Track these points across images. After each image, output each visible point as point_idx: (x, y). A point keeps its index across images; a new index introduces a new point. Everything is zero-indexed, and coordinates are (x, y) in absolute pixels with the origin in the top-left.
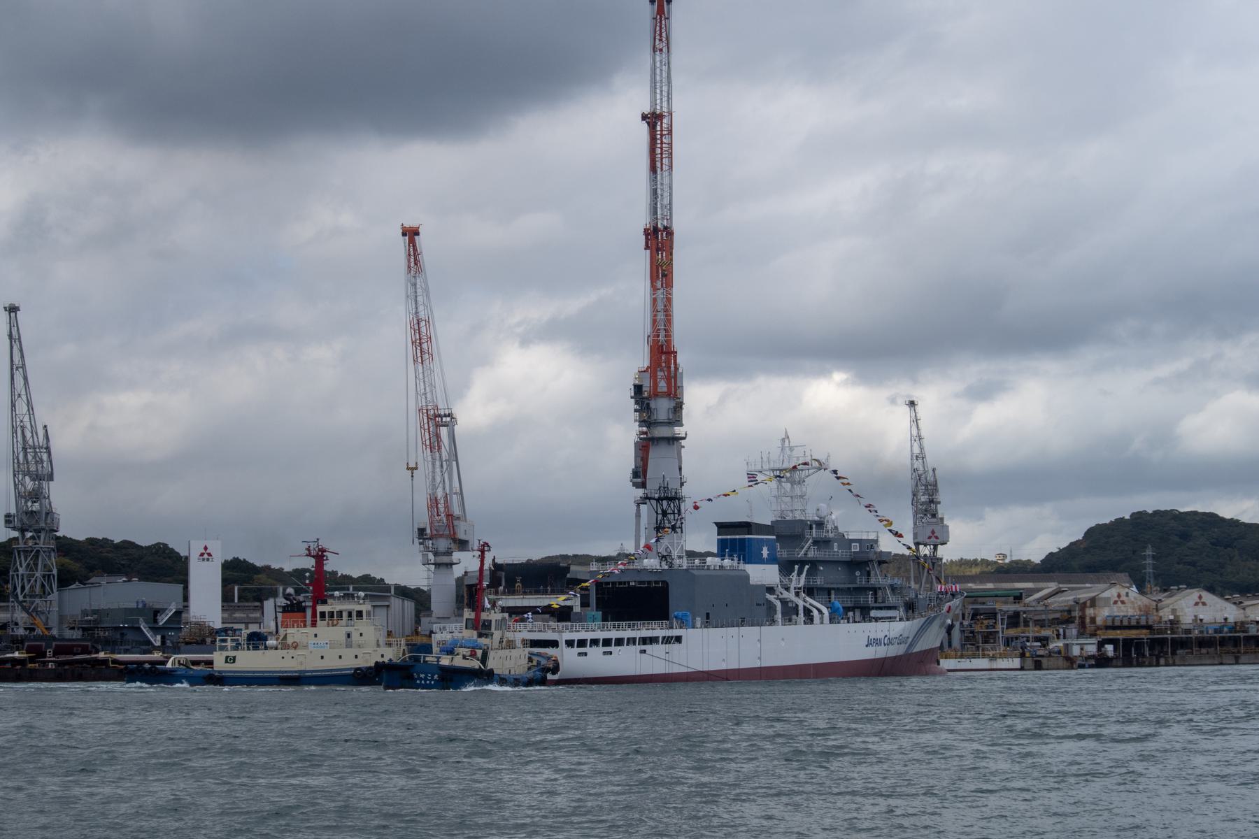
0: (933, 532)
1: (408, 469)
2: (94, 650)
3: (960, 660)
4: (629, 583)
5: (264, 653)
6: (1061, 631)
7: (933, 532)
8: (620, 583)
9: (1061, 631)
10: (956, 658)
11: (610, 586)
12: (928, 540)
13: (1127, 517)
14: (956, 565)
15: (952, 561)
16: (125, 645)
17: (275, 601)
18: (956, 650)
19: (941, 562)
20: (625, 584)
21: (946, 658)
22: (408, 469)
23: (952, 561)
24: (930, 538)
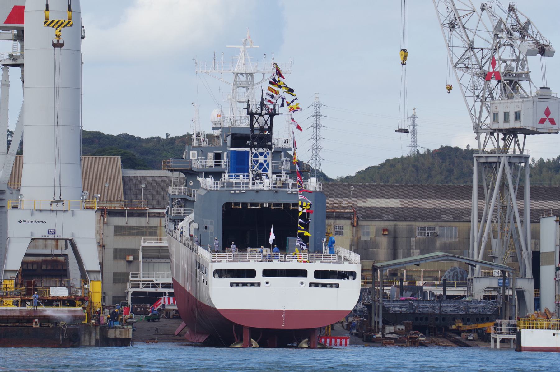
0: (547, 112)
1: (63, 201)
2: (458, 154)
3: (555, 331)
4: (262, 204)
5: (533, 331)
6: (96, 277)
7: (547, 112)
8: (252, 204)
9: (96, 277)
10: (549, 329)
11: (241, 207)
12: (541, 126)
13: (464, 149)
14: (550, 169)
15: (541, 161)
16: (273, 163)
17: (258, 130)
18: (547, 315)
19: (526, 162)
20: (258, 206)
21: (530, 328)
22: (63, 201)
23: (541, 161)
24: (542, 121)
